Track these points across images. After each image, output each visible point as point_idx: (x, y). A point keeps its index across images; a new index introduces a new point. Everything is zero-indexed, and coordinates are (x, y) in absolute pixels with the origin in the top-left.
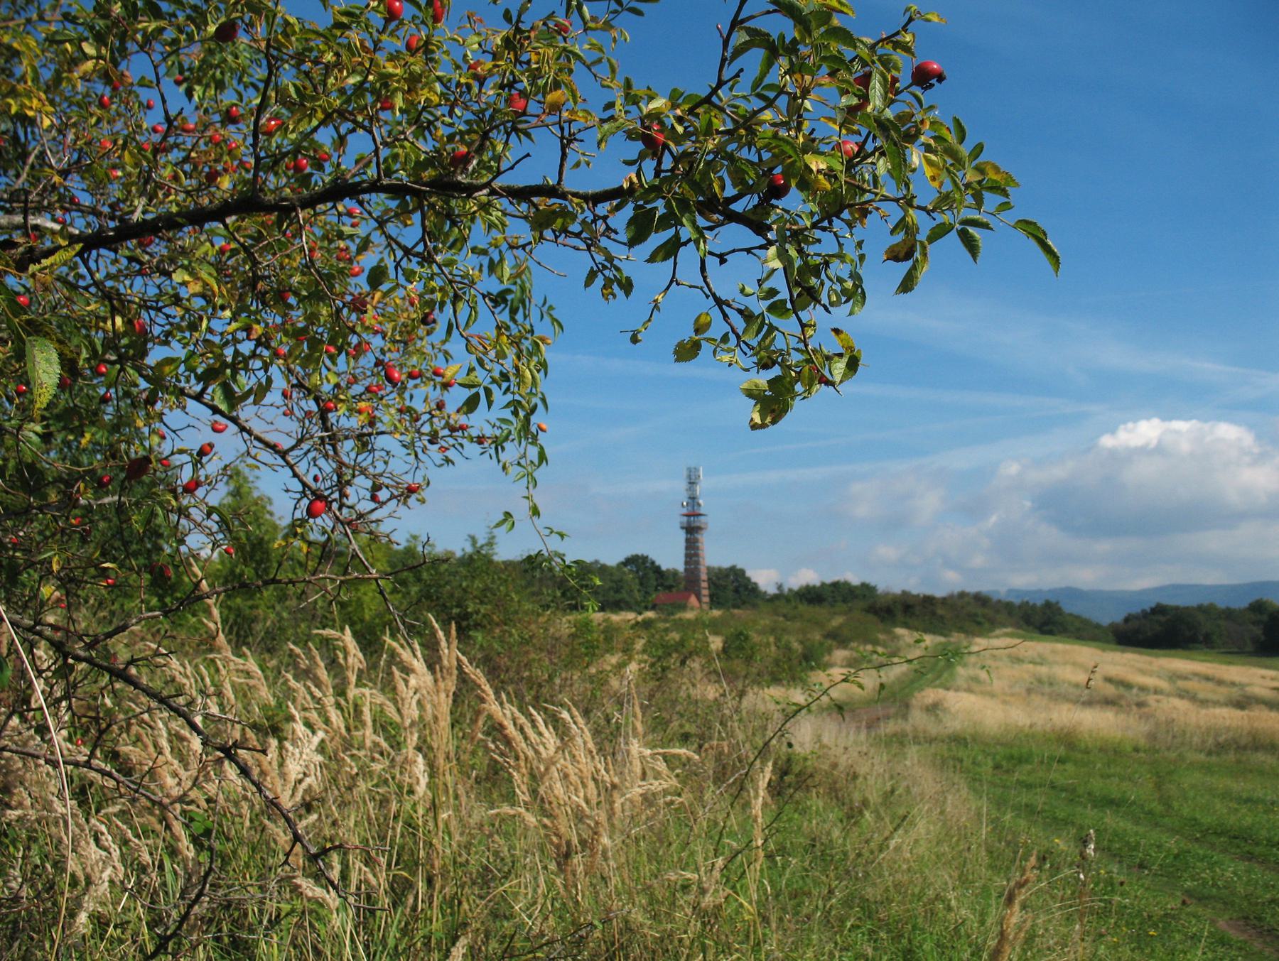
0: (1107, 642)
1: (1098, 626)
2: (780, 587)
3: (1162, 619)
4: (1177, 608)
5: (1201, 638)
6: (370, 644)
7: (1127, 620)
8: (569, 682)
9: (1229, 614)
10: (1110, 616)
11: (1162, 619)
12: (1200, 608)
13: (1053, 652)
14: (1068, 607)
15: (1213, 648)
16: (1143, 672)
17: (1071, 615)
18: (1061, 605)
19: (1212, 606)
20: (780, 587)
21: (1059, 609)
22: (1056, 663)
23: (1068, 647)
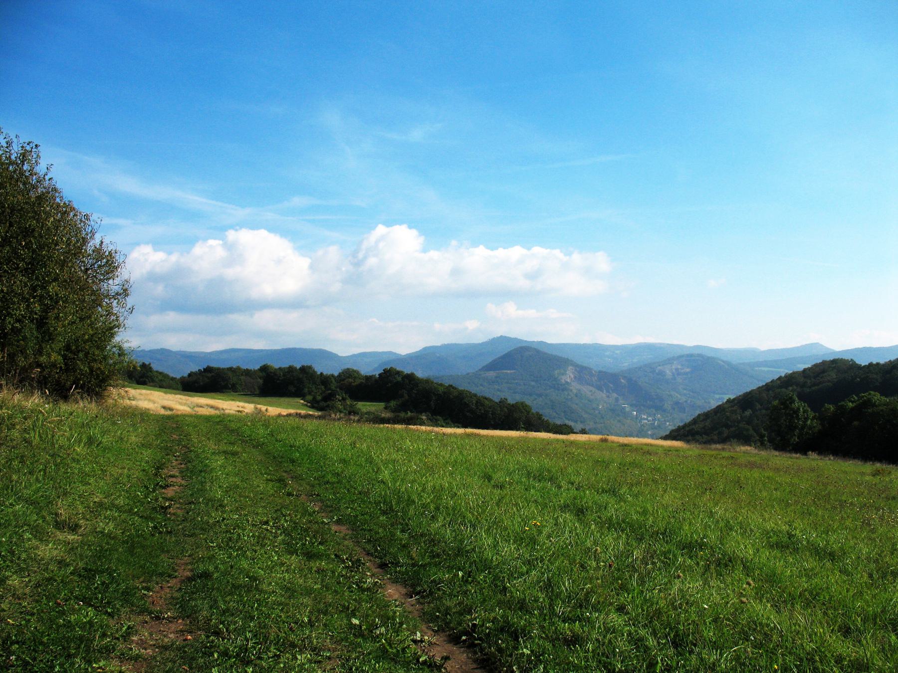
0: (177, 389)
1: (173, 379)
2: (150, 364)
3: (209, 375)
4: (219, 369)
5: (230, 386)
6: (408, 420)
7: (190, 375)
8: (200, 431)
9: (248, 373)
10: (181, 371)
11: (209, 375)
12: (230, 369)
13: (141, 394)
14: (156, 367)
15: (236, 392)
16: (181, 404)
17: (157, 372)
18: (152, 365)
19: (238, 368)
20: (150, 364)
21: (151, 368)
22: (141, 399)
23: (148, 392)
